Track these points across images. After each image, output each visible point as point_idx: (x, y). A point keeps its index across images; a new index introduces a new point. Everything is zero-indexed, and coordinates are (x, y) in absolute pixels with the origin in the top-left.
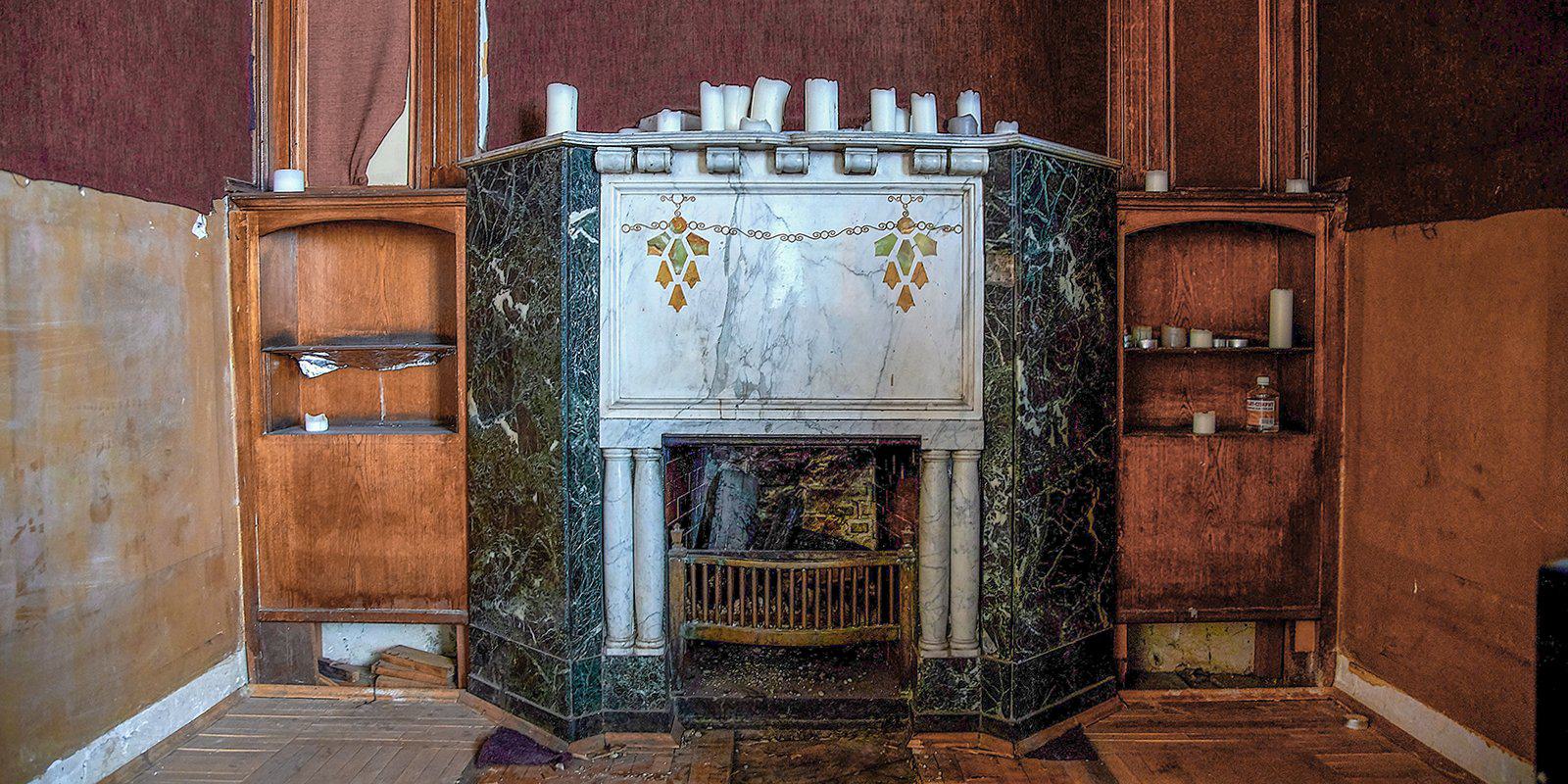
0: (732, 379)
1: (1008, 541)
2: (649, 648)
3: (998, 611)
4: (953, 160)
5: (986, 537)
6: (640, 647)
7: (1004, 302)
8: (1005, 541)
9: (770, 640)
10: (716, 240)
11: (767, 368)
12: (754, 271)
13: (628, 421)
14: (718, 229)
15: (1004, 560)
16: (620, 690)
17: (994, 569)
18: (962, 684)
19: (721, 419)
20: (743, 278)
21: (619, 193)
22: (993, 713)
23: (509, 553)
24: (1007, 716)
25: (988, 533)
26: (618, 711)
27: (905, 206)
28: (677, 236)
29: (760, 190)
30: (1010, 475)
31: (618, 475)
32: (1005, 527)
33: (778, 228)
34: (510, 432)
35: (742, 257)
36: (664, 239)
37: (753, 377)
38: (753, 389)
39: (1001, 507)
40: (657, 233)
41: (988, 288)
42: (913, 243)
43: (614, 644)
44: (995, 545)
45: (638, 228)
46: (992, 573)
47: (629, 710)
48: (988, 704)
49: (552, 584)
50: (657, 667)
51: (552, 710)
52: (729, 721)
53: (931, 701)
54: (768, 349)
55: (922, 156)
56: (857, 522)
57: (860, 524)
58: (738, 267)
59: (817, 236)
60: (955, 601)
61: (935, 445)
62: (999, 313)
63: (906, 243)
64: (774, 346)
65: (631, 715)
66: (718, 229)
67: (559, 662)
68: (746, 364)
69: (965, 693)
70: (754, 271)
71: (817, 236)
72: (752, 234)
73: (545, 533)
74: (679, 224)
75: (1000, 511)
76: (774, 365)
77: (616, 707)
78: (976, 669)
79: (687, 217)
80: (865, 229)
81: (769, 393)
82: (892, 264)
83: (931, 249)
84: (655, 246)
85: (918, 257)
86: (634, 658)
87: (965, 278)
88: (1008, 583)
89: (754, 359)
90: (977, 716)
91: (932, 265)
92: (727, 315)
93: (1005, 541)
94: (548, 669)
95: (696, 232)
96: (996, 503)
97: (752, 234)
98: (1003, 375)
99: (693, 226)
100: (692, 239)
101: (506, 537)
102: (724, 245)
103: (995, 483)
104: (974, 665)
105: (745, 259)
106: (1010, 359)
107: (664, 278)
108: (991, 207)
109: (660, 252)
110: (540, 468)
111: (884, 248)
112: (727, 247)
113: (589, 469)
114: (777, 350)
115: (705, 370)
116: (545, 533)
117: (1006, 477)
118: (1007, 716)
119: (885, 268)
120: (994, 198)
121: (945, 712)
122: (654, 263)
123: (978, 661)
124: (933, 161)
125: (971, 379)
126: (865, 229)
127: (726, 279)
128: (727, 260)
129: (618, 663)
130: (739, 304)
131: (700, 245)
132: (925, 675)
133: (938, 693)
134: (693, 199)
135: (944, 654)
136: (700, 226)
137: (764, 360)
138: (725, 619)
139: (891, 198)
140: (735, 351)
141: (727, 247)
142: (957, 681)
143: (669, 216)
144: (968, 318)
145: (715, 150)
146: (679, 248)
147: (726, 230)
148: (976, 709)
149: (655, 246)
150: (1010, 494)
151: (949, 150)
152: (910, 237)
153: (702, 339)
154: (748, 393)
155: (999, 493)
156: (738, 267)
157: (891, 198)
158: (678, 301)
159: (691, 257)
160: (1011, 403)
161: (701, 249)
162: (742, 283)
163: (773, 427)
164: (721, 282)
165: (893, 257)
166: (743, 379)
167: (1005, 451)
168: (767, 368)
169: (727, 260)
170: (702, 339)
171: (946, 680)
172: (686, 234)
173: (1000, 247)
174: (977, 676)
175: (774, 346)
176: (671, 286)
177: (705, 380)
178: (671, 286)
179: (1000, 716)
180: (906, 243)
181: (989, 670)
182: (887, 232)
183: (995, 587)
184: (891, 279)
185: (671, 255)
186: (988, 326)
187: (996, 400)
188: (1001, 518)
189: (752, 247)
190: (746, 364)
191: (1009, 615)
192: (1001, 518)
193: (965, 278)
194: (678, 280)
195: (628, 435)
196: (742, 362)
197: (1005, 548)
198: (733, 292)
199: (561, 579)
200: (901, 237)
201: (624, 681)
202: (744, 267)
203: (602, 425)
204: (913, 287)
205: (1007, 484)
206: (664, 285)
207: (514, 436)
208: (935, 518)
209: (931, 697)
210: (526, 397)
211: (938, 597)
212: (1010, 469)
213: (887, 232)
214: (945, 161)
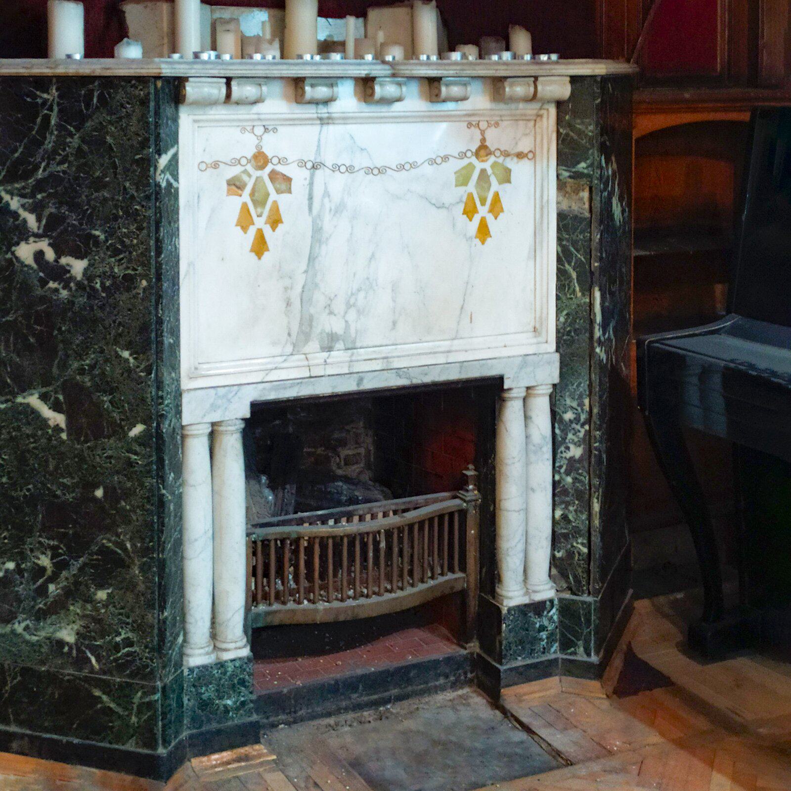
0: (317, 330)
1: (585, 474)
2: (236, 648)
3: (573, 546)
4: (540, 88)
5: (559, 473)
6: (226, 650)
7: (581, 233)
8: (581, 475)
9: (350, 614)
10: (299, 177)
11: (352, 316)
12: (338, 210)
13: (212, 391)
14: (302, 164)
15: (579, 495)
16: (205, 705)
17: (567, 504)
18: (543, 628)
19: (311, 377)
20: (327, 217)
21: (196, 125)
22: (575, 653)
23: (45, 561)
24: (589, 655)
25: (561, 467)
26: (204, 729)
27: (483, 133)
28: (259, 173)
29: (345, 119)
30: (587, 408)
31: (196, 452)
32: (580, 460)
33: (361, 161)
34: (46, 412)
35: (326, 194)
36: (245, 178)
37: (337, 327)
38: (338, 340)
39: (576, 440)
40: (236, 171)
41: (561, 216)
42: (490, 171)
43: (197, 652)
44: (569, 479)
45: (216, 165)
46: (566, 508)
47: (214, 726)
48: (566, 645)
49: (130, 597)
50: (245, 670)
51: (130, 746)
52: (300, 713)
53: (515, 652)
54: (352, 294)
55: (511, 85)
56: (350, 452)
57: (354, 455)
58: (322, 205)
59: (401, 167)
60: (533, 542)
61: (515, 384)
62: (574, 243)
63: (483, 171)
64: (359, 290)
65: (219, 732)
66: (302, 164)
67: (143, 687)
68: (331, 313)
69: (544, 637)
70: (338, 210)
71: (401, 167)
72: (336, 168)
73: (118, 535)
74: (260, 159)
75: (575, 444)
76: (358, 311)
77: (200, 727)
78: (554, 610)
79: (269, 152)
80: (445, 158)
81: (354, 342)
82: (470, 196)
83: (506, 177)
84: (235, 185)
85: (495, 186)
86: (221, 665)
87: (538, 206)
88: (584, 517)
89: (339, 306)
90: (556, 660)
91: (507, 194)
92: (312, 259)
93: (581, 475)
94: (123, 694)
95: (280, 168)
96: (570, 436)
97: (336, 168)
98: (578, 306)
99: (275, 161)
100: (273, 176)
101: (40, 543)
102: (307, 182)
103: (569, 416)
104: (552, 606)
105: (329, 196)
106: (588, 290)
107: (244, 221)
108: (567, 135)
109: (240, 192)
110: (110, 457)
111: (463, 178)
112: (311, 184)
113: (162, 450)
114: (361, 295)
115: (289, 323)
116: (118, 535)
117: (582, 410)
118: (589, 655)
119: (464, 199)
120: (570, 126)
121: (529, 662)
122: (235, 203)
123: (556, 602)
124: (520, 89)
125: (545, 311)
126: (445, 158)
127: (310, 220)
128: (311, 198)
129: (204, 674)
130: (324, 247)
131: (283, 182)
132: (509, 625)
133: (521, 642)
134: (275, 130)
135: (526, 600)
136: (282, 161)
137: (349, 306)
138: (278, 597)
139: (470, 125)
140: (319, 298)
141: (311, 184)
142: (537, 625)
143: (250, 152)
144: (542, 247)
145: (313, 81)
146: (260, 188)
147: (309, 165)
148: (554, 652)
149: (235, 185)
150: (587, 427)
151: (536, 78)
152: (487, 165)
153: (286, 289)
154: (333, 344)
155: (574, 425)
156: (322, 205)
157: (470, 125)
158: (260, 246)
159: (273, 196)
160: (587, 335)
161: (284, 187)
162: (327, 223)
163: (365, 381)
164: (305, 224)
165: (471, 187)
166: (328, 330)
167: (580, 383)
168: (352, 316)
169: (311, 198)
170: (286, 289)
171: (527, 627)
172: (269, 168)
173: (577, 176)
174: (555, 617)
175: (359, 290)
176: (252, 230)
177: (289, 335)
178: (252, 230)
179: (581, 656)
180: (483, 171)
181: (566, 609)
182: (466, 162)
183: (569, 521)
184: (470, 211)
185: (252, 194)
186: (561, 255)
187: (570, 332)
188: (576, 452)
189: (338, 183)
190: (331, 313)
191: (585, 550)
192: (576, 452)
193: (538, 206)
194: (260, 223)
195: (214, 407)
196: (327, 311)
197: (580, 481)
198: (317, 231)
199: (148, 588)
200: (479, 165)
201: (208, 693)
202: (327, 205)
203: (185, 399)
204: (490, 218)
205: (583, 417)
206: (245, 229)
207: (57, 419)
208: (517, 460)
209: (513, 647)
210: (81, 371)
211: (519, 541)
212: (587, 401)
213: (466, 162)
214: (532, 89)
